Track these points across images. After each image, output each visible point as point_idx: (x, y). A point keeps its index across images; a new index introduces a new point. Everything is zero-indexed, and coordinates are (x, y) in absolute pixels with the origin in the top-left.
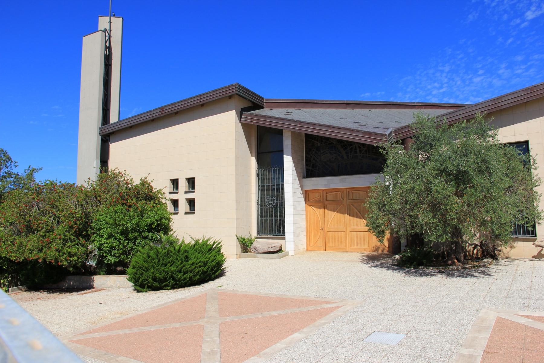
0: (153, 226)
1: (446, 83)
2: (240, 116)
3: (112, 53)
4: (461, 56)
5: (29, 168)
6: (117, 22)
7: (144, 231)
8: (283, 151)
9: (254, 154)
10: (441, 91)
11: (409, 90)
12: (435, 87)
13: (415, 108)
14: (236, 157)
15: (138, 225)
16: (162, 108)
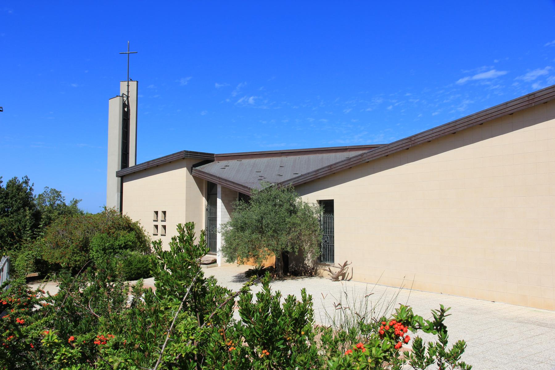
0: (122, 246)
2: (191, 171)
5: (73, 199)
6: (133, 85)
14: (186, 199)
15: (112, 245)
16: (148, 162)
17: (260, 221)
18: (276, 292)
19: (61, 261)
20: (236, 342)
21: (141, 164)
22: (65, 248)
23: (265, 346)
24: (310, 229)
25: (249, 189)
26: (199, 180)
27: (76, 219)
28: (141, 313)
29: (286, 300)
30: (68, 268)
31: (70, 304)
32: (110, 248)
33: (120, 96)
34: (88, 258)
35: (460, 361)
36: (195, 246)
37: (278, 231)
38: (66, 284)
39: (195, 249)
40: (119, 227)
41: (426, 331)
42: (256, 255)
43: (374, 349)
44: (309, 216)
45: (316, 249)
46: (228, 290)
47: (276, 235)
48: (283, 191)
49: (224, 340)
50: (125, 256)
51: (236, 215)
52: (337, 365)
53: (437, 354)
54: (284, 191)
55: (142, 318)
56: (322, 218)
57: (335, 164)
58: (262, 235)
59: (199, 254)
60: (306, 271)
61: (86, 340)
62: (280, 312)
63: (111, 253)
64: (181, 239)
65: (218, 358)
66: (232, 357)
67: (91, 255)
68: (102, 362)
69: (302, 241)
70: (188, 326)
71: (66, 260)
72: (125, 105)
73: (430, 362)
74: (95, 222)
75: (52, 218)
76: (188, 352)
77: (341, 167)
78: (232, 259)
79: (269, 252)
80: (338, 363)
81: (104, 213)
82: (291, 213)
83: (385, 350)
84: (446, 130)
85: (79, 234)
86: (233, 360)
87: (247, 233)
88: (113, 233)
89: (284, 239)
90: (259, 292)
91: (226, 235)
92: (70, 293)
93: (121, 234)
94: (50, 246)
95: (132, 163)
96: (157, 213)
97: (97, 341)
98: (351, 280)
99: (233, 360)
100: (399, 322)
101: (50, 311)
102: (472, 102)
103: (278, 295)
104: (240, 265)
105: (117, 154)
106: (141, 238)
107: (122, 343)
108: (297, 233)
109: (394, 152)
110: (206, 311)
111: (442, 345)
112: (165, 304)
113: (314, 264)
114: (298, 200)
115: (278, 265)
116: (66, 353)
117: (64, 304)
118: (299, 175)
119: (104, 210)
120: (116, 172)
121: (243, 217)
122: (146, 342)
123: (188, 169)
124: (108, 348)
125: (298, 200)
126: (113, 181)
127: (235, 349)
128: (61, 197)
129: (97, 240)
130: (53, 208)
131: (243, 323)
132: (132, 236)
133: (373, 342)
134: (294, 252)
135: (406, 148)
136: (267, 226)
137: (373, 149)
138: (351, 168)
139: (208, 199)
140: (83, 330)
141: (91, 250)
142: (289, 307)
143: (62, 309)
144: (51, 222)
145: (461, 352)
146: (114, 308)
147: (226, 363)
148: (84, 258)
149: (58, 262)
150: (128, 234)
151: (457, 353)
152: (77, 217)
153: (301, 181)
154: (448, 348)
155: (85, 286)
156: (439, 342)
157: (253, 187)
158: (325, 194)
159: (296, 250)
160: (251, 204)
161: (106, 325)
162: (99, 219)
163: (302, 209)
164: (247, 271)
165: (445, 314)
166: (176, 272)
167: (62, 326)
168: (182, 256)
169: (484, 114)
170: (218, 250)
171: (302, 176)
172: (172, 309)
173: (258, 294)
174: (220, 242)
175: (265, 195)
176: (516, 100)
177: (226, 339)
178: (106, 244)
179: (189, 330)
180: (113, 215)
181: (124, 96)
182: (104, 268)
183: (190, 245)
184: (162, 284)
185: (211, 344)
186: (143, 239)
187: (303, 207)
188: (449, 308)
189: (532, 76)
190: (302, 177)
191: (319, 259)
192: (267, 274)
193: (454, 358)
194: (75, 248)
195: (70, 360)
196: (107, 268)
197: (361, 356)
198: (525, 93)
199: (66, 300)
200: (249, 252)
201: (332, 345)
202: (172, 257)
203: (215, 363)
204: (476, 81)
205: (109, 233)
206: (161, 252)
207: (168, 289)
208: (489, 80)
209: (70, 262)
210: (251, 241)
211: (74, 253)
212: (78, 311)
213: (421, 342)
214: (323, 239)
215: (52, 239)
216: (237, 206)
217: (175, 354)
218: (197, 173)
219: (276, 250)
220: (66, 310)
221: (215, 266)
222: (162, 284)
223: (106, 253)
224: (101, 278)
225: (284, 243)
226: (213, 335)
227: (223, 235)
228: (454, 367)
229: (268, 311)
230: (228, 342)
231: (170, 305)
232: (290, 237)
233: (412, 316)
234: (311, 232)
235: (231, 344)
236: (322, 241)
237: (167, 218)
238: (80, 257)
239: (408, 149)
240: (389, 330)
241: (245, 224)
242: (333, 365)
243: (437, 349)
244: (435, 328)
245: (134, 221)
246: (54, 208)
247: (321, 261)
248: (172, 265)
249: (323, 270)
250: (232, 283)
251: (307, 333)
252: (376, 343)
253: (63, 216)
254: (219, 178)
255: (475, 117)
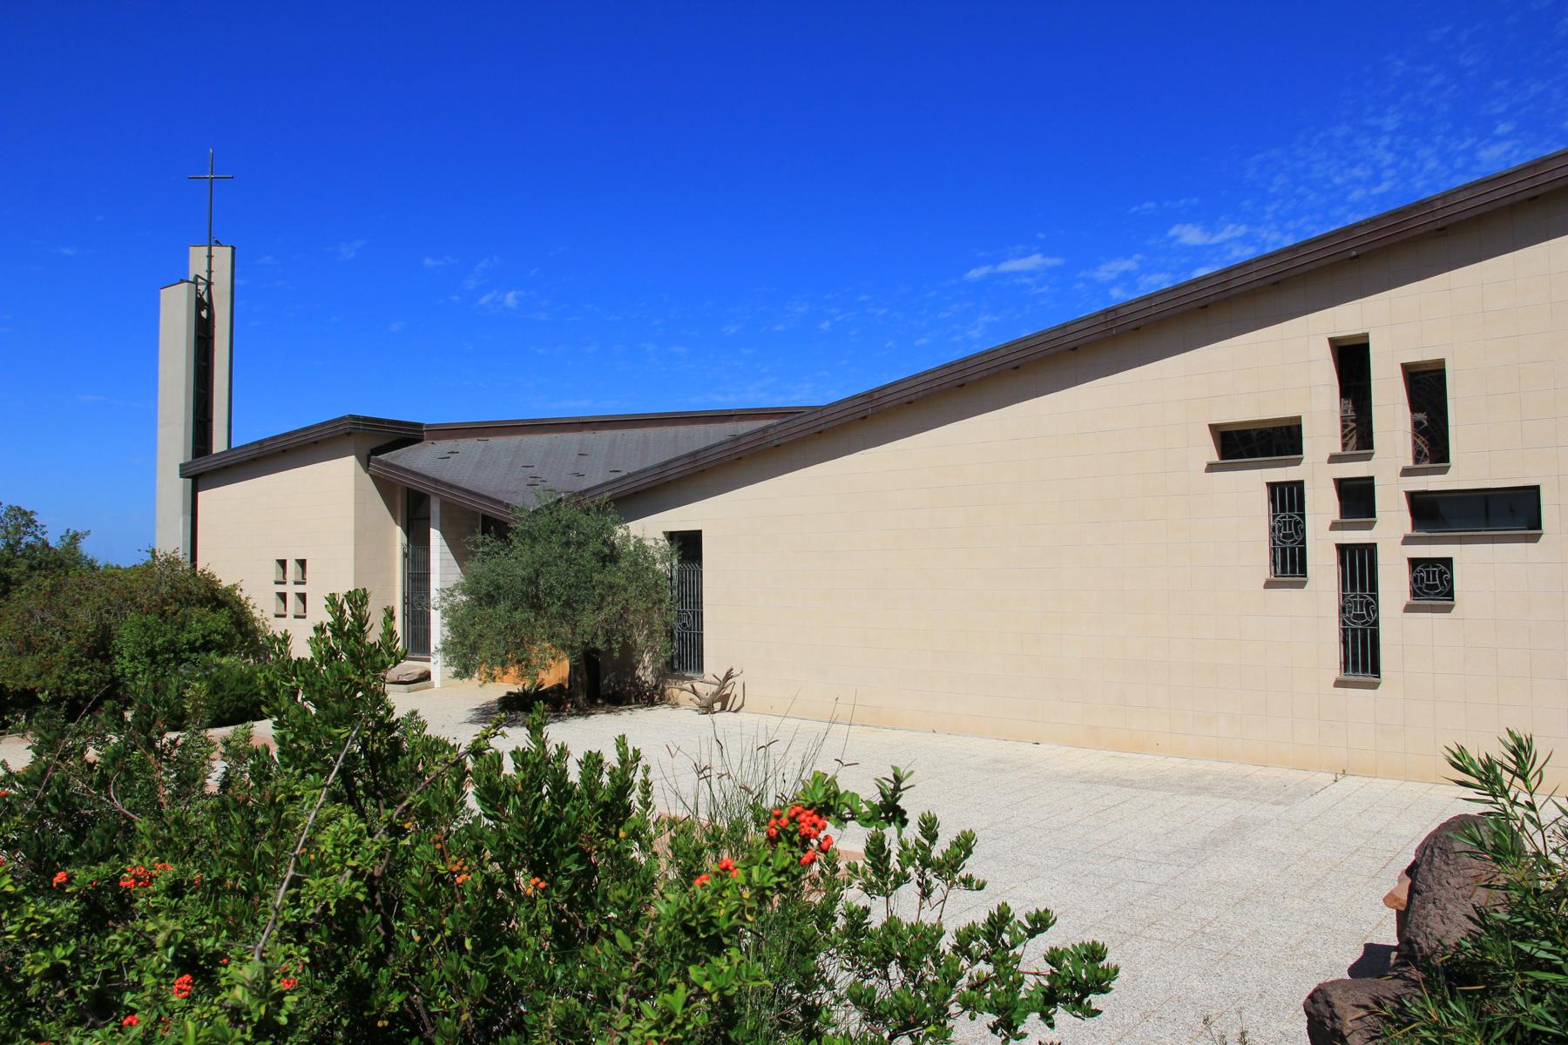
0: (197, 644)
1: (1391, 166)
2: (365, 462)
3: (213, 315)
4: (1436, 81)
5: (68, 532)
6: (223, 255)
7: (184, 651)
8: (429, 519)
9: (399, 521)
10: (1376, 191)
11: (1273, 190)
12: (1356, 181)
13: (731, 420)
15: (172, 642)
16: (260, 442)
17: (533, 581)
18: (557, 746)
19: (40, 683)
20: (474, 863)
21: (242, 447)
22: (50, 652)
23: (537, 870)
24: (647, 598)
25: (507, 506)
26: (385, 486)
27: (77, 580)
28: (241, 805)
29: (580, 763)
30: (56, 702)
31: (62, 791)
32: (167, 650)
33: (188, 281)
34: (109, 676)
35: (963, 874)
36: (372, 645)
37: (574, 605)
38: (49, 742)
39: (372, 652)
40: (188, 599)
41: (864, 823)
42: (523, 660)
43: (755, 870)
44: (647, 568)
45: (661, 641)
46: (452, 745)
47: (569, 612)
48: (587, 512)
49: (444, 860)
50: (206, 668)
51: (475, 566)
52: (676, 909)
53: (917, 863)
54: (589, 509)
55: (243, 817)
56: (675, 573)
57: (705, 449)
58: (537, 614)
59: (380, 663)
60: (640, 693)
61: (98, 879)
62: (569, 793)
63: (169, 661)
64: (338, 630)
65: (432, 901)
66: (464, 898)
67: (118, 668)
68: (128, 934)
69: (631, 626)
70: (343, 837)
71: (51, 681)
72: (203, 305)
73: (902, 879)
74: (126, 588)
75: (14, 577)
76: (342, 896)
77: (719, 456)
78: (467, 671)
79: (553, 651)
80: (678, 905)
81: (149, 567)
82: (604, 562)
83: (779, 869)
84: (946, 380)
85: (84, 617)
86: (466, 903)
87: (503, 607)
88: (175, 613)
89: (590, 620)
90: (518, 748)
91: (451, 614)
92: (59, 763)
93: (195, 617)
94: (9, 647)
95: (219, 444)
96: (283, 563)
97: (127, 881)
98: (743, 709)
99: (466, 903)
100: (810, 807)
101: (8, 811)
102: (996, 319)
103: (563, 752)
104: (485, 682)
105: (182, 421)
106: (246, 623)
107: (191, 883)
108: (619, 607)
109: (834, 424)
110: (400, 796)
111: (927, 842)
112: (287, 788)
113: (657, 678)
114: (620, 532)
115: (575, 680)
116: (37, 917)
117: (45, 791)
118: (624, 473)
119: (151, 559)
120: (181, 465)
121: (493, 571)
122: (253, 874)
123: (359, 459)
124: (156, 894)
125: (620, 532)
126: (172, 487)
127: (469, 878)
128: (36, 526)
129: (131, 631)
130: (14, 554)
131: (486, 821)
132: (221, 620)
133: (754, 855)
134: (611, 650)
135: (861, 415)
136: (550, 593)
137: (790, 417)
138: (740, 458)
139: (408, 531)
140: (94, 852)
141: (117, 657)
142: (589, 779)
143: (40, 803)
144: (11, 587)
145: (966, 856)
146: (176, 796)
147: (450, 911)
148: (101, 675)
149: (31, 686)
150: (213, 615)
151: (957, 857)
152: (80, 575)
153: (627, 487)
154: (937, 853)
155: (104, 742)
156: (920, 836)
157: (516, 501)
158: (681, 518)
159: (616, 646)
160: (511, 541)
161: (154, 837)
162: (137, 581)
163: (630, 551)
164: (504, 698)
165: (902, 786)
166: (326, 707)
167: (41, 846)
168: (339, 671)
169: (1021, 346)
170: (433, 649)
171: (629, 475)
172: (305, 800)
173: (514, 754)
174: (438, 630)
175: (546, 520)
176: (1082, 320)
177: (450, 857)
178: (157, 639)
179: (344, 846)
180: (173, 570)
181: (200, 280)
182: (146, 702)
183: (358, 643)
184: (292, 736)
185: (415, 872)
186: (249, 628)
187: (632, 548)
188: (911, 773)
189: (1110, 272)
190: (630, 480)
191: (669, 664)
192: (538, 707)
193: (952, 867)
194: (77, 651)
195: (50, 931)
196: (156, 703)
197: (728, 888)
198: (1098, 307)
199: (48, 782)
200: (507, 653)
201: (690, 859)
202: (315, 673)
203: (424, 913)
204: (1005, 275)
205: (162, 615)
206: (288, 661)
207: (307, 748)
208: (1031, 274)
209: (63, 684)
210: (512, 629)
211: (72, 664)
212: (81, 807)
213: (882, 841)
214: (679, 619)
215: (15, 630)
216: (477, 547)
217: (311, 904)
218: (380, 469)
219: (571, 647)
220: (50, 805)
221: (427, 688)
222: (292, 736)
223: (155, 663)
224: (141, 725)
225: (588, 630)
226: (417, 849)
227: (444, 614)
228: (951, 887)
229: (540, 789)
230: (454, 865)
231: (299, 790)
232: (601, 617)
233: (836, 795)
234: (650, 605)
235: (462, 867)
236: (677, 625)
237: (308, 576)
238: (90, 674)
239: (865, 418)
240: (787, 826)
241: (498, 587)
242: (667, 910)
243: (916, 853)
244: (883, 815)
245: (225, 584)
246: (19, 553)
247: (673, 670)
248: (315, 691)
249: (675, 690)
250: (468, 725)
251: (635, 835)
252: (760, 856)
253: (44, 572)
254: (436, 481)
255: (1003, 352)
